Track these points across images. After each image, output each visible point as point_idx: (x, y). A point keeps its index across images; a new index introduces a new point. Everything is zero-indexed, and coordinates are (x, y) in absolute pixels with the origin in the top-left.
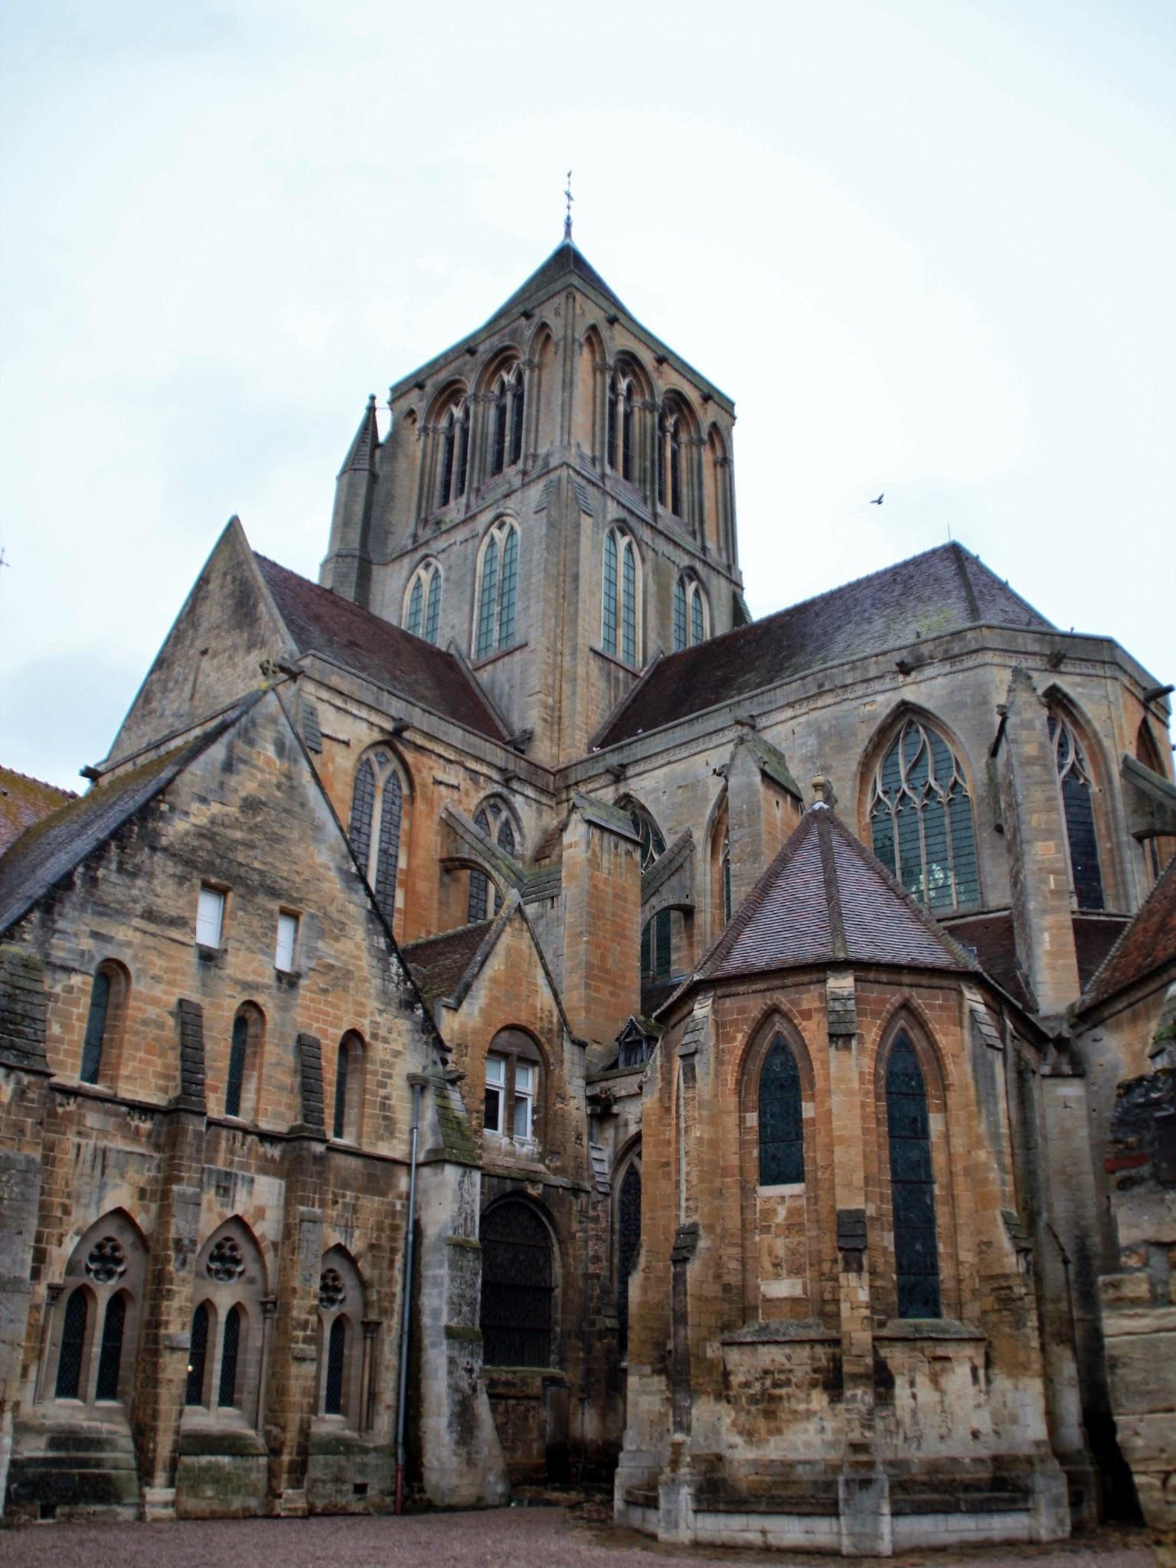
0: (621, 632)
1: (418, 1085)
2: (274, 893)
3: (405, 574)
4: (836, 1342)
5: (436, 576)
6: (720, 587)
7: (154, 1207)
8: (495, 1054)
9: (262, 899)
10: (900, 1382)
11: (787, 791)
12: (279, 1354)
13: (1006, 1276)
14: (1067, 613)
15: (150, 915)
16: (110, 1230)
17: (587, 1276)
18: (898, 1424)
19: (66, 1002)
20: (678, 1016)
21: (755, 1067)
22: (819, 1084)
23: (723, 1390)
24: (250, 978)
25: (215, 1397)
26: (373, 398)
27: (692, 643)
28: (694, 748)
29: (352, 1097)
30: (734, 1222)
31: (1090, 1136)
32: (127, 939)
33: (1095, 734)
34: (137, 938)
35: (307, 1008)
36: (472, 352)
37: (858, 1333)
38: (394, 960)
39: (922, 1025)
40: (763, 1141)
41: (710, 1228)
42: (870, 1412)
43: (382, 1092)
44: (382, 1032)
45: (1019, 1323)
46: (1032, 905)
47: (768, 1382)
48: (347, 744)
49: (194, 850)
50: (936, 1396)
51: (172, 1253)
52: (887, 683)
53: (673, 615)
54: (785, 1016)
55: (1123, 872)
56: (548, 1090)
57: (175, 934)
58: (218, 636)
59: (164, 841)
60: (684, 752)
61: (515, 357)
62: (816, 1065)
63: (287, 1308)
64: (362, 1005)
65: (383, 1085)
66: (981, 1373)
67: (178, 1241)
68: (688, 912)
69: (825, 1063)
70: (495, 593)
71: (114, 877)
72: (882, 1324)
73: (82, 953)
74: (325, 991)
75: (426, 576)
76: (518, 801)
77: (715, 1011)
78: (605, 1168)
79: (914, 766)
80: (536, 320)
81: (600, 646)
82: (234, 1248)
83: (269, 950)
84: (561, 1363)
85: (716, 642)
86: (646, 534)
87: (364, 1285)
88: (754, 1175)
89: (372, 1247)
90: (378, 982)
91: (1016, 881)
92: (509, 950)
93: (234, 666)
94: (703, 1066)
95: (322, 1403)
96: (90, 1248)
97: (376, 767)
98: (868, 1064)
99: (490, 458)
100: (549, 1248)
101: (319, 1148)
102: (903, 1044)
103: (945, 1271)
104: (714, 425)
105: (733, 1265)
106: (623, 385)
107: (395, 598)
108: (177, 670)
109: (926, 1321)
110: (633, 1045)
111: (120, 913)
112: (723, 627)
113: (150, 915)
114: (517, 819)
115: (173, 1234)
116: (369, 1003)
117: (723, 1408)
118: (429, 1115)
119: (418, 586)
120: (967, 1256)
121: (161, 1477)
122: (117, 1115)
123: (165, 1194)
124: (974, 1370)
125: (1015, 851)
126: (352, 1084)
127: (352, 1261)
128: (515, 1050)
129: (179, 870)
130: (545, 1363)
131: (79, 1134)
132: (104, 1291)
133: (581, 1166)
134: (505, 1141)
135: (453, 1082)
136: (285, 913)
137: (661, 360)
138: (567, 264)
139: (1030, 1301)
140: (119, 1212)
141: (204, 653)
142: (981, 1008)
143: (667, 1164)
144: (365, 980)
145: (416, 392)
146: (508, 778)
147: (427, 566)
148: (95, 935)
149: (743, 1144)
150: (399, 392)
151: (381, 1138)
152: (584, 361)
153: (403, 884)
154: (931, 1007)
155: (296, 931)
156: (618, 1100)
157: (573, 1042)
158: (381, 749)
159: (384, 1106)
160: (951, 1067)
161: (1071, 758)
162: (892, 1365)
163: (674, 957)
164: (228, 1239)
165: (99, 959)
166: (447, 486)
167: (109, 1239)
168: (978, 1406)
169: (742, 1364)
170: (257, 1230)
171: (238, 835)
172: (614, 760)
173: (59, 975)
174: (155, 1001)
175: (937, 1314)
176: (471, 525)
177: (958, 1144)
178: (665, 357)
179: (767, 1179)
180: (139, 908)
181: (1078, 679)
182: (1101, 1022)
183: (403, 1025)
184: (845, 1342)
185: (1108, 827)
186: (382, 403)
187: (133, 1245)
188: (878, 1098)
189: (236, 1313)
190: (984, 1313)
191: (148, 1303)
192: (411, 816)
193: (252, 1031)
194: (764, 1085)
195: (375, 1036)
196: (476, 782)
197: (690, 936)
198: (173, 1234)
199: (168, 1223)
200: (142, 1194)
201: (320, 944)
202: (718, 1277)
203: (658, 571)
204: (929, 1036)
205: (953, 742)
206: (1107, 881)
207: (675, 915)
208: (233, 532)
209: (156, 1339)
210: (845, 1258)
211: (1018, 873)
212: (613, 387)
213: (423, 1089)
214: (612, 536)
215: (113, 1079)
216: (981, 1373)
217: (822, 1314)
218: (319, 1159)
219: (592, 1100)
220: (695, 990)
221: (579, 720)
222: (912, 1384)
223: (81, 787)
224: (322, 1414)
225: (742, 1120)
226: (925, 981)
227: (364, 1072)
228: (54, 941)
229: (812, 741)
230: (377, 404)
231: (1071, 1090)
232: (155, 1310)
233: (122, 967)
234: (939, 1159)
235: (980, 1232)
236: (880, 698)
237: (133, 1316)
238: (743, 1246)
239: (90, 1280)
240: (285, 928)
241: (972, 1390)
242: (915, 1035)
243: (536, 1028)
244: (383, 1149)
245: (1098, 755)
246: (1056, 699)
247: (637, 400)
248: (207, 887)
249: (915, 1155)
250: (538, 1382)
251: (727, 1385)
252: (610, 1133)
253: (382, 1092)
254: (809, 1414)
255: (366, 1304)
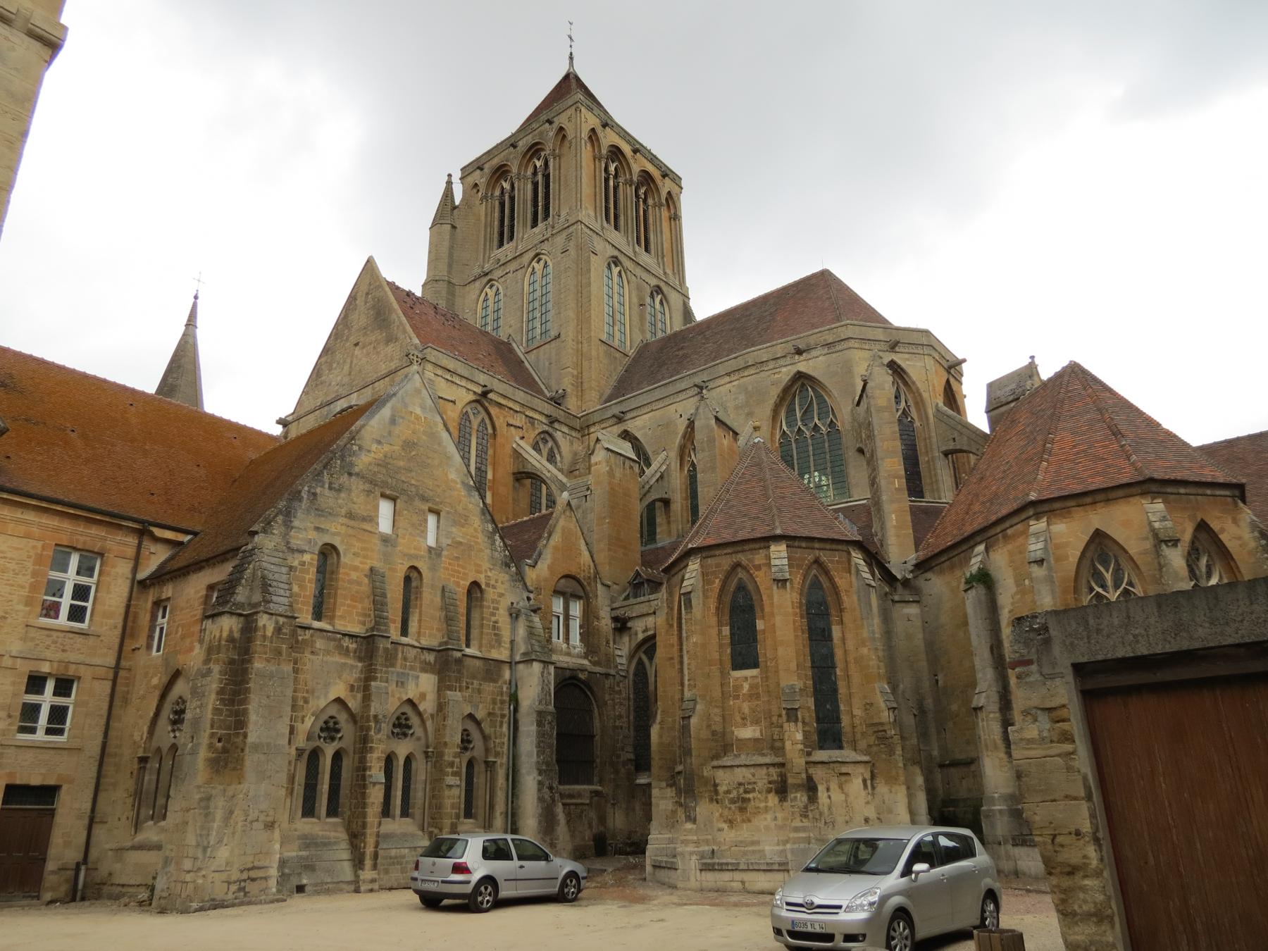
0: (616, 328)
1: (514, 615)
2: (424, 499)
3: (477, 292)
4: (783, 765)
5: (497, 293)
6: (674, 297)
7: (359, 696)
8: (557, 592)
9: (418, 503)
10: (821, 788)
11: (730, 429)
12: (436, 782)
13: (882, 724)
14: (899, 314)
15: (350, 515)
16: (333, 711)
17: (615, 728)
18: (821, 814)
19: (301, 571)
20: (677, 569)
21: (728, 599)
22: (767, 609)
23: (714, 797)
24: (413, 552)
25: (398, 812)
26: (450, 175)
27: (660, 335)
28: (667, 402)
29: (475, 623)
30: (717, 693)
31: (924, 638)
32: (336, 531)
33: (918, 390)
34: (343, 530)
35: (447, 569)
36: (514, 146)
37: (797, 760)
38: (497, 537)
39: (827, 572)
40: (733, 644)
41: (703, 697)
42: (806, 807)
43: (493, 619)
44: (492, 582)
45: (891, 752)
46: (884, 498)
47: (741, 790)
48: (454, 402)
49: (375, 474)
50: (843, 797)
51: (373, 724)
52: (788, 361)
53: (648, 317)
54: (745, 568)
55: (936, 475)
56: (589, 616)
57: (367, 526)
58: (365, 334)
59: (357, 469)
60: (661, 404)
61: (543, 150)
62: (764, 598)
63: (441, 755)
64: (479, 566)
65: (494, 614)
66: (869, 782)
67: (376, 717)
68: (666, 503)
69: (771, 597)
70: (537, 304)
71: (327, 492)
72: (809, 754)
73: (310, 541)
74: (457, 558)
75: (491, 293)
76: (558, 435)
77: (702, 566)
78: (624, 661)
79: (806, 412)
80: (555, 126)
81: (604, 337)
82: (407, 719)
83: (424, 532)
84: (601, 782)
85: (675, 335)
86: (627, 263)
87: (486, 738)
88: (728, 665)
89: (490, 714)
90: (488, 551)
91: (873, 482)
92: (563, 529)
93: (378, 353)
94: (696, 600)
95: (462, 813)
96: (320, 723)
97: (472, 417)
98: (796, 596)
99: (529, 216)
100: (591, 711)
101: (459, 655)
102: (816, 585)
103: (845, 721)
104: (669, 193)
105: (718, 719)
106: (612, 168)
107: (475, 307)
108: (339, 356)
109: (837, 752)
110: (638, 585)
111: (332, 514)
112: (678, 325)
113: (350, 515)
114: (558, 447)
115: (372, 713)
116: (485, 563)
117: (714, 806)
118: (521, 631)
119: (486, 300)
120: (857, 712)
121: (368, 862)
122: (334, 640)
123: (366, 688)
124: (864, 781)
125: (872, 463)
126: (475, 615)
127: (478, 723)
128: (569, 590)
129: (367, 486)
130: (590, 782)
131: (312, 652)
132: (329, 750)
133: (609, 660)
134: (565, 646)
135: (535, 611)
136: (431, 511)
137: (635, 151)
138: (570, 86)
139: (897, 739)
140: (339, 701)
141: (356, 345)
142: (862, 562)
143: (672, 658)
144: (481, 550)
145: (478, 172)
146: (552, 421)
147: (491, 287)
148: (317, 529)
149: (721, 646)
150: (466, 171)
151: (493, 647)
152: (586, 152)
153: (491, 488)
154: (832, 562)
155: (438, 521)
156: (630, 619)
157: (603, 584)
158: (474, 405)
159: (494, 628)
160: (845, 598)
161: (903, 404)
162: (816, 778)
163: (658, 530)
164: (403, 714)
165: (320, 544)
166: (501, 234)
167: (332, 717)
168: (868, 803)
169: (725, 780)
170: (421, 708)
171: (401, 463)
172: (616, 410)
173: (296, 555)
174: (356, 569)
175: (841, 748)
176: (519, 261)
177: (850, 645)
178: (638, 149)
179: (735, 668)
180: (343, 511)
181: (907, 356)
182: (930, 569)
183: (504, 577)
184: (789, 766)
185: (926, 446)
186: (456, 179)
187: (347, 721)
188: (802, 617)
189: (408, 760)
190: (869, 746)
191: (357, 756)
192: (494, 446)
193: (414, 584)
194: (733, 610)
195: (488, 585)
196: (533, 424)
197: (668, 517)
198: (372, 713)
199: (369, 706)
200: (352, 688)
201: (454, 530)
202: (709, 726)
203: (639, 288)
204: (831, 579)
205: (830, 396)
206: (926, 481)
207: (658, 504)
208: (370, 268)
209: (364, 778)
210: (787, 714)
211: (875, 478)
212: (606, 169)
213: (517, 617)
214: (609, 267)
215: (331, 619)
216: (869, 782)
217: (772, 748)
218: (459, 661)
219: (615, 619)
220: (689, 553)
221: (594, 384)
222: (828, 790)
223: (277, 430)
224: (462, 819)
225: (720, 631)
226: (828, 546)
227: (481, 607)
228: (292, 533)
229: (742, 397)
230: (453, 180)
231: (913, 610)
232: (363, 760)
233: (334, 548)
234: (839, 653)
235: (865, 697)
236: (784, 370)
237: (347, 764)
238: (723, 708)
239: (321, 743)
240: (432, 520)
241: (863, 793)
242: (823, 579)
243: (581, 576)
244: (494, 654)
245: (920, 403)
246: (893, 365)
247: (621, 180)
248: (384, 496)
249: (824, 651)
250: (588, 794)
251: (716, 792)
252: (626, 639)
253: (493, 619)
254: (767, 809)
255: (487, 750)
